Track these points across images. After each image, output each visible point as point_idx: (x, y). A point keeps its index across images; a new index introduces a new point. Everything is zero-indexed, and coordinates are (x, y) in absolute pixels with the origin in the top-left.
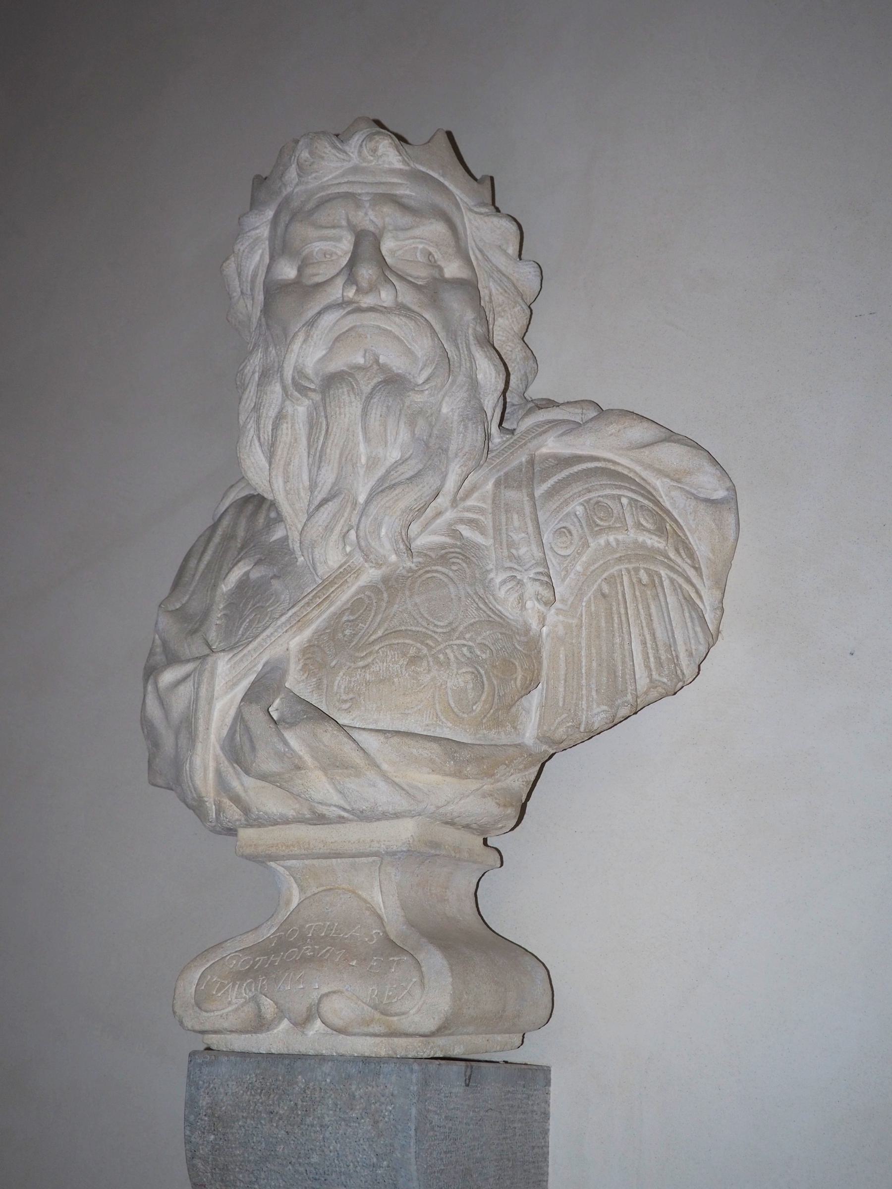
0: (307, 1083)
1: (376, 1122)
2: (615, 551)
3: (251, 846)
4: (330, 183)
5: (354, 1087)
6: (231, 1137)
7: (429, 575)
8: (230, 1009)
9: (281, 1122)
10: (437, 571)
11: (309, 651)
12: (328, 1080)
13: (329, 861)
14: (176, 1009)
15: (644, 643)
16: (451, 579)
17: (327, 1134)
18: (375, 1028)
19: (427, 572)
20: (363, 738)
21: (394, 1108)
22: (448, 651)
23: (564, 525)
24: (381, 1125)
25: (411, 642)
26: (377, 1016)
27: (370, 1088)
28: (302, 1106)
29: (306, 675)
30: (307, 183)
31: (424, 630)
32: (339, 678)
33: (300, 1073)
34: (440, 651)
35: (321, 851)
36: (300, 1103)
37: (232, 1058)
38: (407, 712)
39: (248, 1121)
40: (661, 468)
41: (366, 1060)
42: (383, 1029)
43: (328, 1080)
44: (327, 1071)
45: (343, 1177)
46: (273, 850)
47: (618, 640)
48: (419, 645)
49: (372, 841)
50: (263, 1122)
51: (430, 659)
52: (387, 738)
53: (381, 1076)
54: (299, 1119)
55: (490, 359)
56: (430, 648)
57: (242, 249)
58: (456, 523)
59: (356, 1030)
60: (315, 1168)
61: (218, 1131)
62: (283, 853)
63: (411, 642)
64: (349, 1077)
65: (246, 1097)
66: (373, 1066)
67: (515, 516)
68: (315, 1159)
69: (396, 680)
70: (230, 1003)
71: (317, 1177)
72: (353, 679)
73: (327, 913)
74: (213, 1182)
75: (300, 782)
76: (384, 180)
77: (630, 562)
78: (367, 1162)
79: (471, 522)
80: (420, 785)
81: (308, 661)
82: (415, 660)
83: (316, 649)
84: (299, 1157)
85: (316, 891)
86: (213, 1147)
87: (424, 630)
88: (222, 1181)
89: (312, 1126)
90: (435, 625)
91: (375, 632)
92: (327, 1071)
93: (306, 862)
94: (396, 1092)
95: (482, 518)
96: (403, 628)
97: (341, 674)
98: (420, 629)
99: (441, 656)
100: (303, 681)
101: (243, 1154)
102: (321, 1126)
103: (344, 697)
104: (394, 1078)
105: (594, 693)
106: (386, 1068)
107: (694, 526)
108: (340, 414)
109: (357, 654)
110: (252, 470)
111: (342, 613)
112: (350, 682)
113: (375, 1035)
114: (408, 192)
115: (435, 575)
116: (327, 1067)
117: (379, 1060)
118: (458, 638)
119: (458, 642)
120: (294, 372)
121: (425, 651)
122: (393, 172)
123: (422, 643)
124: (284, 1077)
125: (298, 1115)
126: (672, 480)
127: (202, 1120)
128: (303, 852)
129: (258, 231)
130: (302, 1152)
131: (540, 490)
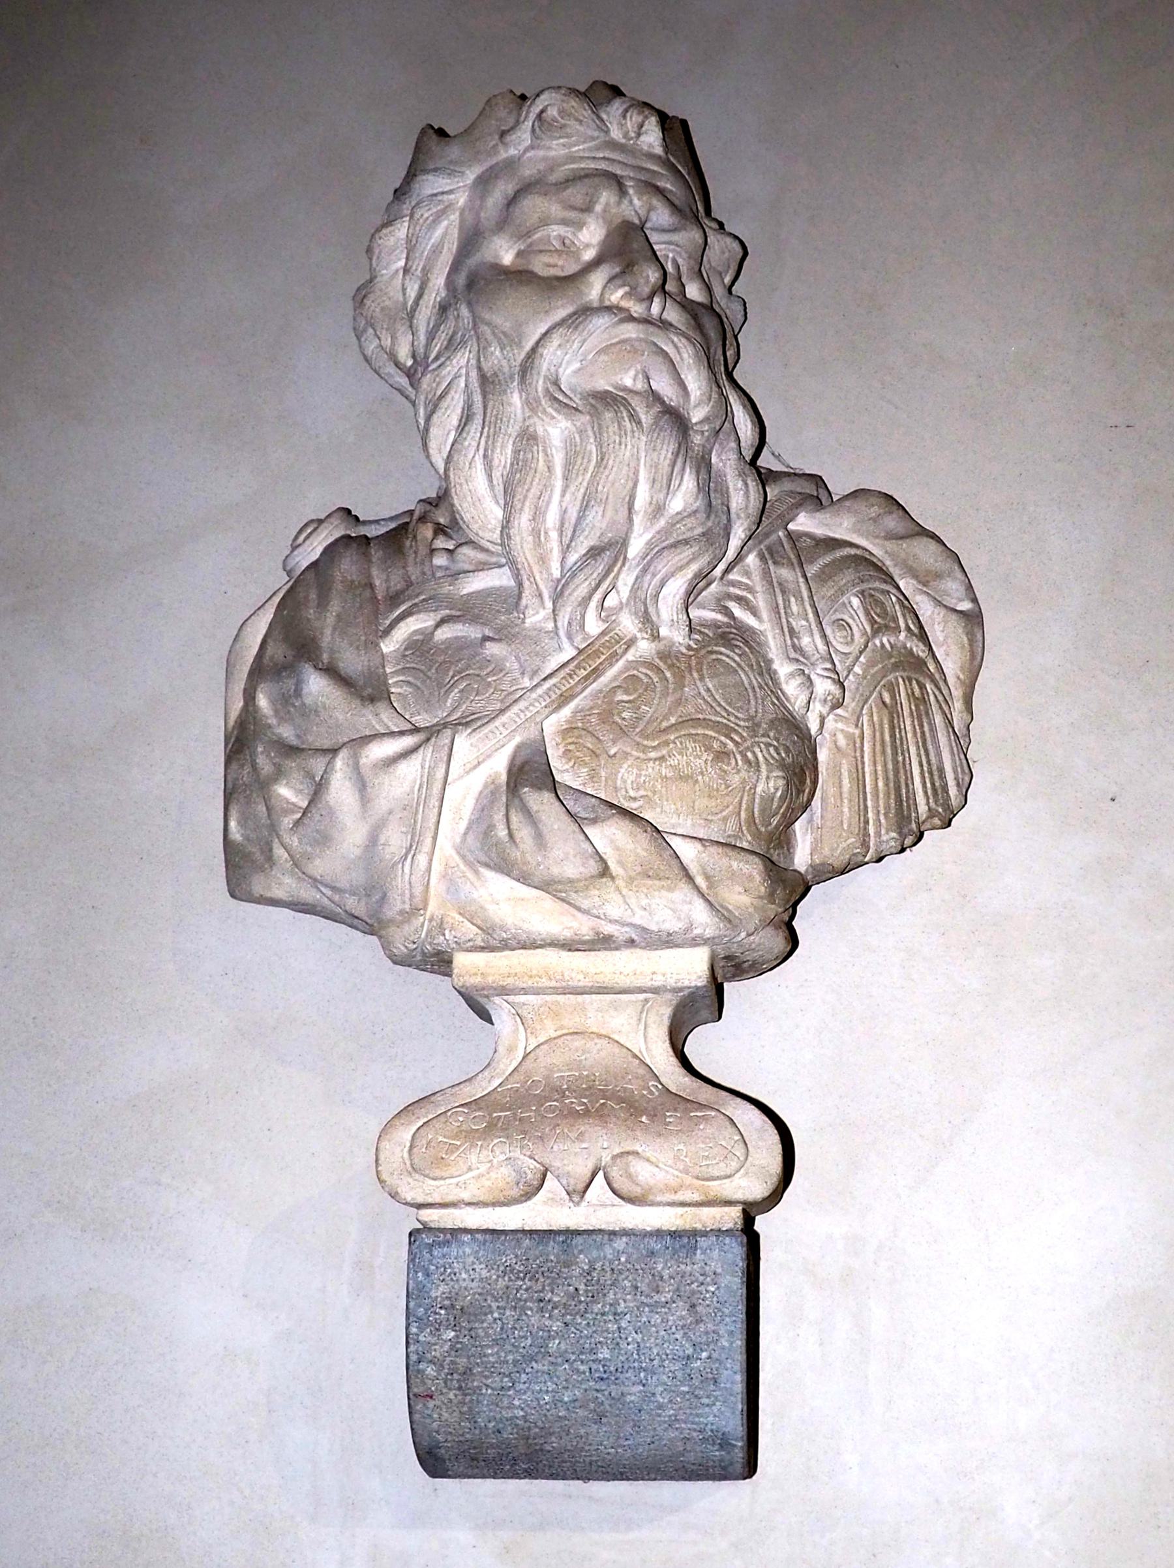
0: (591, 1264)
1: (693, 1306)
2: (890, 656)
3: (475, 974)
4: (581, 154)
5: (660, 1267)
6: (481, 1333)
7: (714, 656)
8: (470, 1174)
9: (556, 1311)
10: (721, 653)
11: (567, 731)
12: (623, 1259)
13: (580, 998)
14: (384, 1177)
15: (921, 765)
16: (739, 665)
17: (624, 1324)
18: (688, 1196)
19: (711, 652)
20: (675, 842)
21: (718, 1288)
22: (757, 750)
23: (840, 616)
24: (699, 1309)
25: (713, 734)
26: (688, 1180)
27: (683, 1267)
28: (586, 1291)
29: (571, 763)
30: (550, 148)
31: (725, 721)
32: (622, 771)
33: (581, 1252)
34: (747, 749)
35: (581, 984)
36: (582, 1287)
37: (478, 1236)
38: (710, 817)
39: (508, 1313)
40: (914, 565)
41: (675, 1234)
42: (696, 1197)
43: (623, 1259)
44: (621, 1249)
45: (642, 1375)
46: (510, 981)
47: (900, 759)
48: (723, 738)
49: (654, 973)
50: (529, 1313)
51: (739, 757)
52: (704, 846)
53: (699, 1251)
54: (582, 1307)
55: (744, 407)
56: (736, 744)
57: (426, 215)
58: (724, 598)
59: (659, 1199)
60: (604, 1366)
61: (461, 1327)
62: (524, 985)
63: (713, 734)
64: (652, 1253)
65: (501, 1283)
66: (686, 1240)
67: (793, 599)
68: (604, 1353)
69: (700, 778)
70: (470, 1169)
71: (605, 1376)
72: (643, 773)
73: (580, 1061)
74: (445, 1391)
75: (597, 892)
76: (644, 165)
77: (904, 670)
78: (681, 1354)
79: (739, 600)
80: (730, 907)
81: (571, 747)
82: (722, 755)
83: (584, 733)
84: (582, 1353)
85: (554, 1035)
86: (452, 1348)
87: (725, 721)
88: (460, 1388)
89: (603, 1314)
90: (736, 717)
91: (666, 718)
92: (621, 1249)
93: (548, 998)
94: (719, 1271)
95: (749, 596)
96: (700, 716)
97: (625, 766)
98: (718, 719)
99: (749, 754)
100: (567, 771)
101: (497, 1353)
102: (615, 1314)
103: (632, 793)
104: (715, 1254)
105: (882, 818)
106: (703, 1242)
107: (941, 639)
108: (620, 444)
109: (645, 743)
110: (469, 499)
111: (614, 690)
112: (638, 776)
113: (683, 1204)
114: (668, 186)
115: (724, 658)
116: (620, 1243)
117: (694, 1233)
118: (763, 736)
119: (763, 740)
120: (544, 382)
121: (731, 745)
122: (651, 156)
123: (727, 736)
124: (557, 1256)
125: (581, 1302)
126: (920, 582)
127: (436, 1313)
128: (553, 984)
129: (452, 197)
130: (587, 1346)
131: (812, 570)
